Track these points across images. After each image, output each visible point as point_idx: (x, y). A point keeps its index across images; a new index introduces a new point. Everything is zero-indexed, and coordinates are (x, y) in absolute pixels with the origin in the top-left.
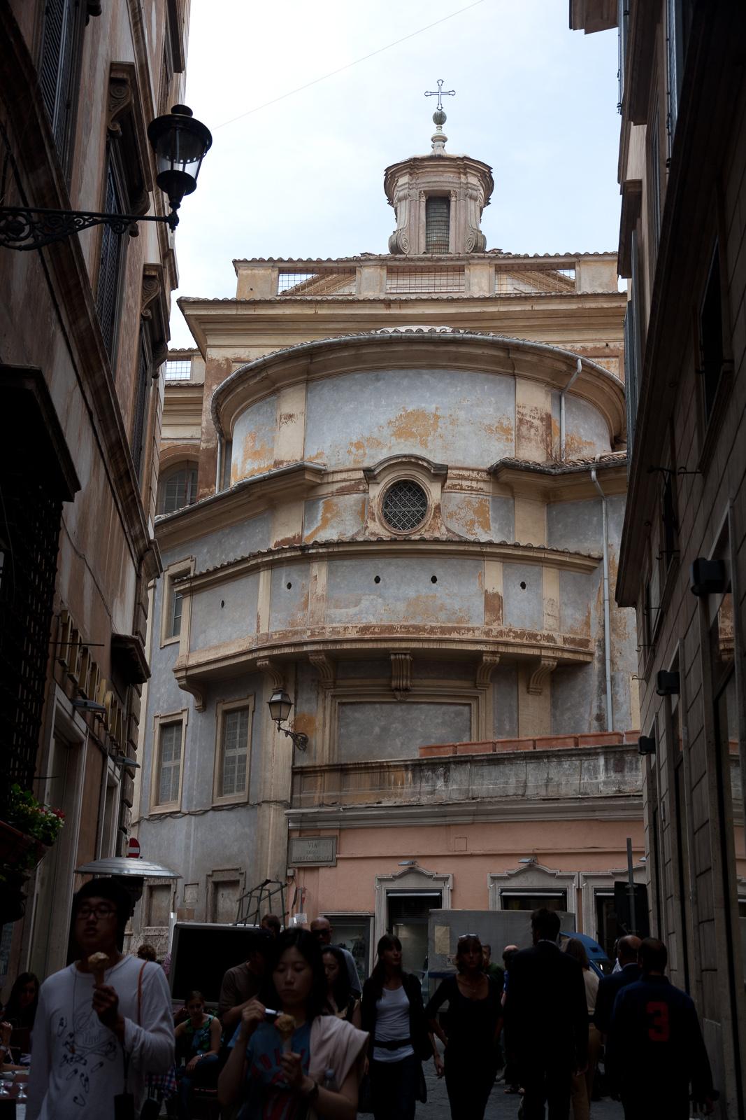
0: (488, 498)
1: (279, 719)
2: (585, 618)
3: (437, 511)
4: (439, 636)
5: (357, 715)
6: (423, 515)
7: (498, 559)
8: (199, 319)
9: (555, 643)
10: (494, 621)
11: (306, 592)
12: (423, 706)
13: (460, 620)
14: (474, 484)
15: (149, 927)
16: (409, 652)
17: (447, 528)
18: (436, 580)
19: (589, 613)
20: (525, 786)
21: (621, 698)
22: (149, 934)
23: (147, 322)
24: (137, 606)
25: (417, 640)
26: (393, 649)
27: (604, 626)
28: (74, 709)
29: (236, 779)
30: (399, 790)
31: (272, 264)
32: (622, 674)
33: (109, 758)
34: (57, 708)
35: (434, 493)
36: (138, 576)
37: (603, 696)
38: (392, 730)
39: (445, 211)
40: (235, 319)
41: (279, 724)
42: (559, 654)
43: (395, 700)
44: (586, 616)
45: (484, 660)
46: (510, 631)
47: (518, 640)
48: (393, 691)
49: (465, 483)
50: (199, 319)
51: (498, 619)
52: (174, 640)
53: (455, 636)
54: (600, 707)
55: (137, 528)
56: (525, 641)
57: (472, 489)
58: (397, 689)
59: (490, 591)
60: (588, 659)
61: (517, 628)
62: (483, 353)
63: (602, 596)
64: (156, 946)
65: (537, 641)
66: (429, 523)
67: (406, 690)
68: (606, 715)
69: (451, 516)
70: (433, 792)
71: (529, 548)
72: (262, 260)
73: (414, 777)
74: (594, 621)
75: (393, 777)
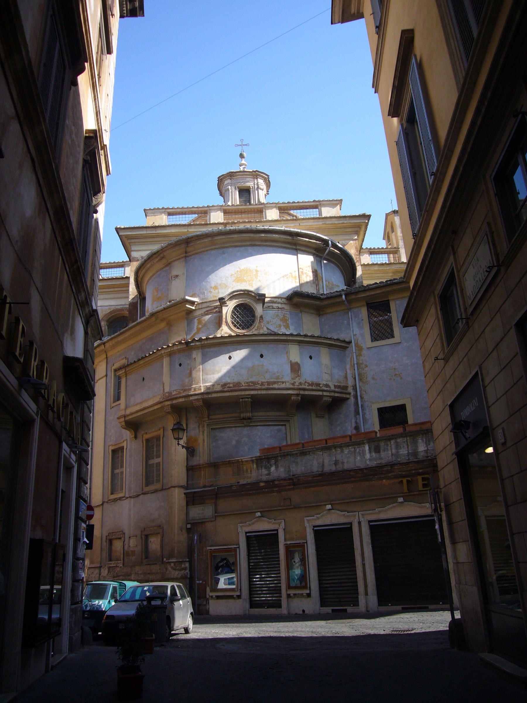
0: (287, 313)
1: (178, 439)
2: (344, 374)
3: (261, 319)
4: (266, 386)
5: (222, 435)
6: (253, 322)
7: (296, 343)
8: (127, 237)
9: (330, 388)
10: (297, 377)
11: (190, 367)
12: (259, 427)
13: (278, 378)
14: (280, 306)
15: (111, 562)
16: (250, 397)
17: (267, 328)
18: (263, 356)
19: (347, 372)
20: (323, 465)
21: (367, 416)
22: (111, 566)
23: (87, 165)
24: (86, 352)
25: (254, 389)
26: (241, 395)
27: (355, 378)
28: (21, 386)
29: (155, 476)
31: (164, 210)
32: (367, 403)
33: (64, 444)
34: (64, 455)
35: (259, 309)
36: (86, 333)
37: (358, 416)
39: (248, 195)
40: (146, 236)
41: (178, 442)
42: (333, 394)
43: (243, 425)
45: (292, 400)
46: (306, 382)
47: (310, 387)
48: (242, 420)
49: (275, 305)
50: (129, 237)
51: (299, 376)
52: (118, 403)
53: (276, 386)
54: (356, 422)
55: (83, 294)
56: (314, 388)
57: (278, 308)
58: (244, 419)
59: (293, 361)
60: (348, 396)
61: (309, 380)
62: (280, 237)
63: (352, 362)
64: (115, 572)
65: (320, 387)
66: (257, 325)
67: (249, 418)
68: (360, 426)
69: (268, 323)
70: (269, 474)
71: (312, 337)
72: (158, 209)
73: (257, 467)
74: (349, 376)
75: (245, 467)
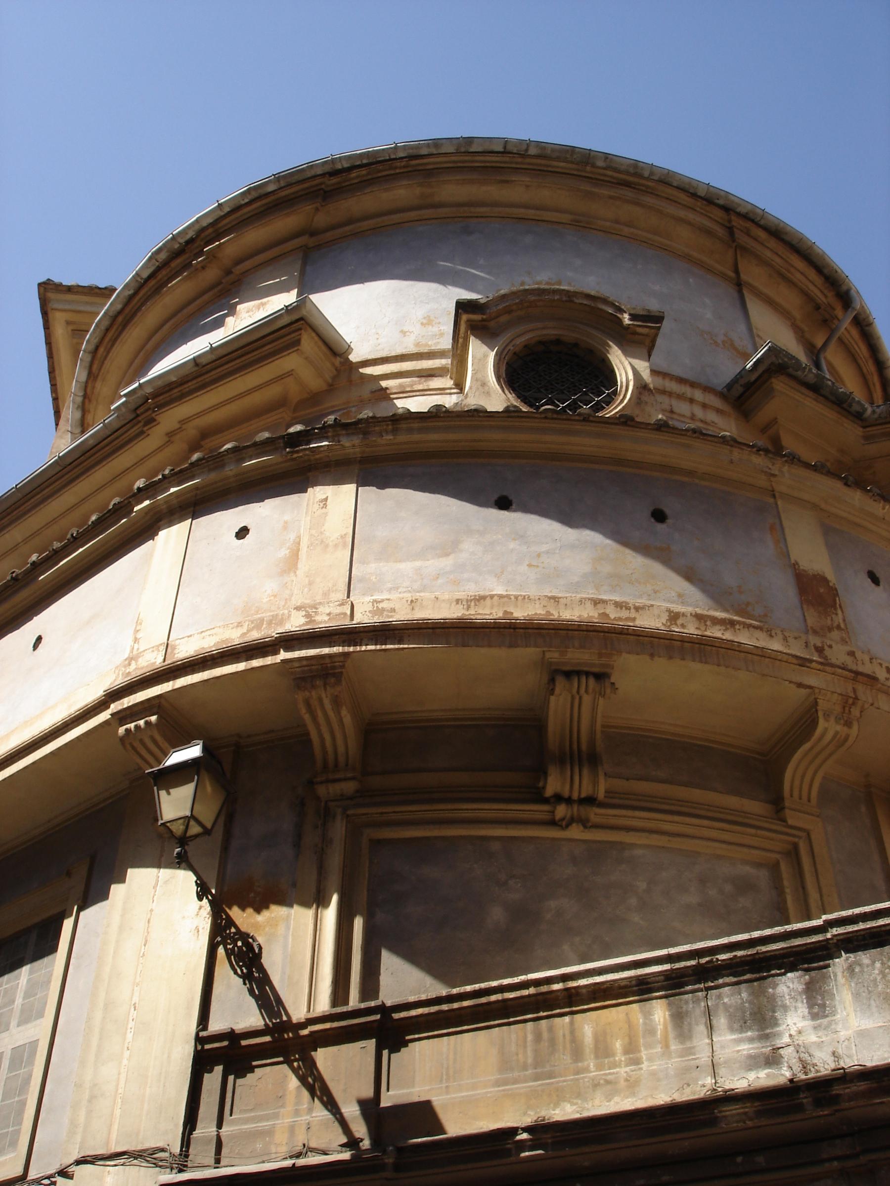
11: (292, 536)
30: (623, 1071)
38: (548, 916)
44: (740, 999)
